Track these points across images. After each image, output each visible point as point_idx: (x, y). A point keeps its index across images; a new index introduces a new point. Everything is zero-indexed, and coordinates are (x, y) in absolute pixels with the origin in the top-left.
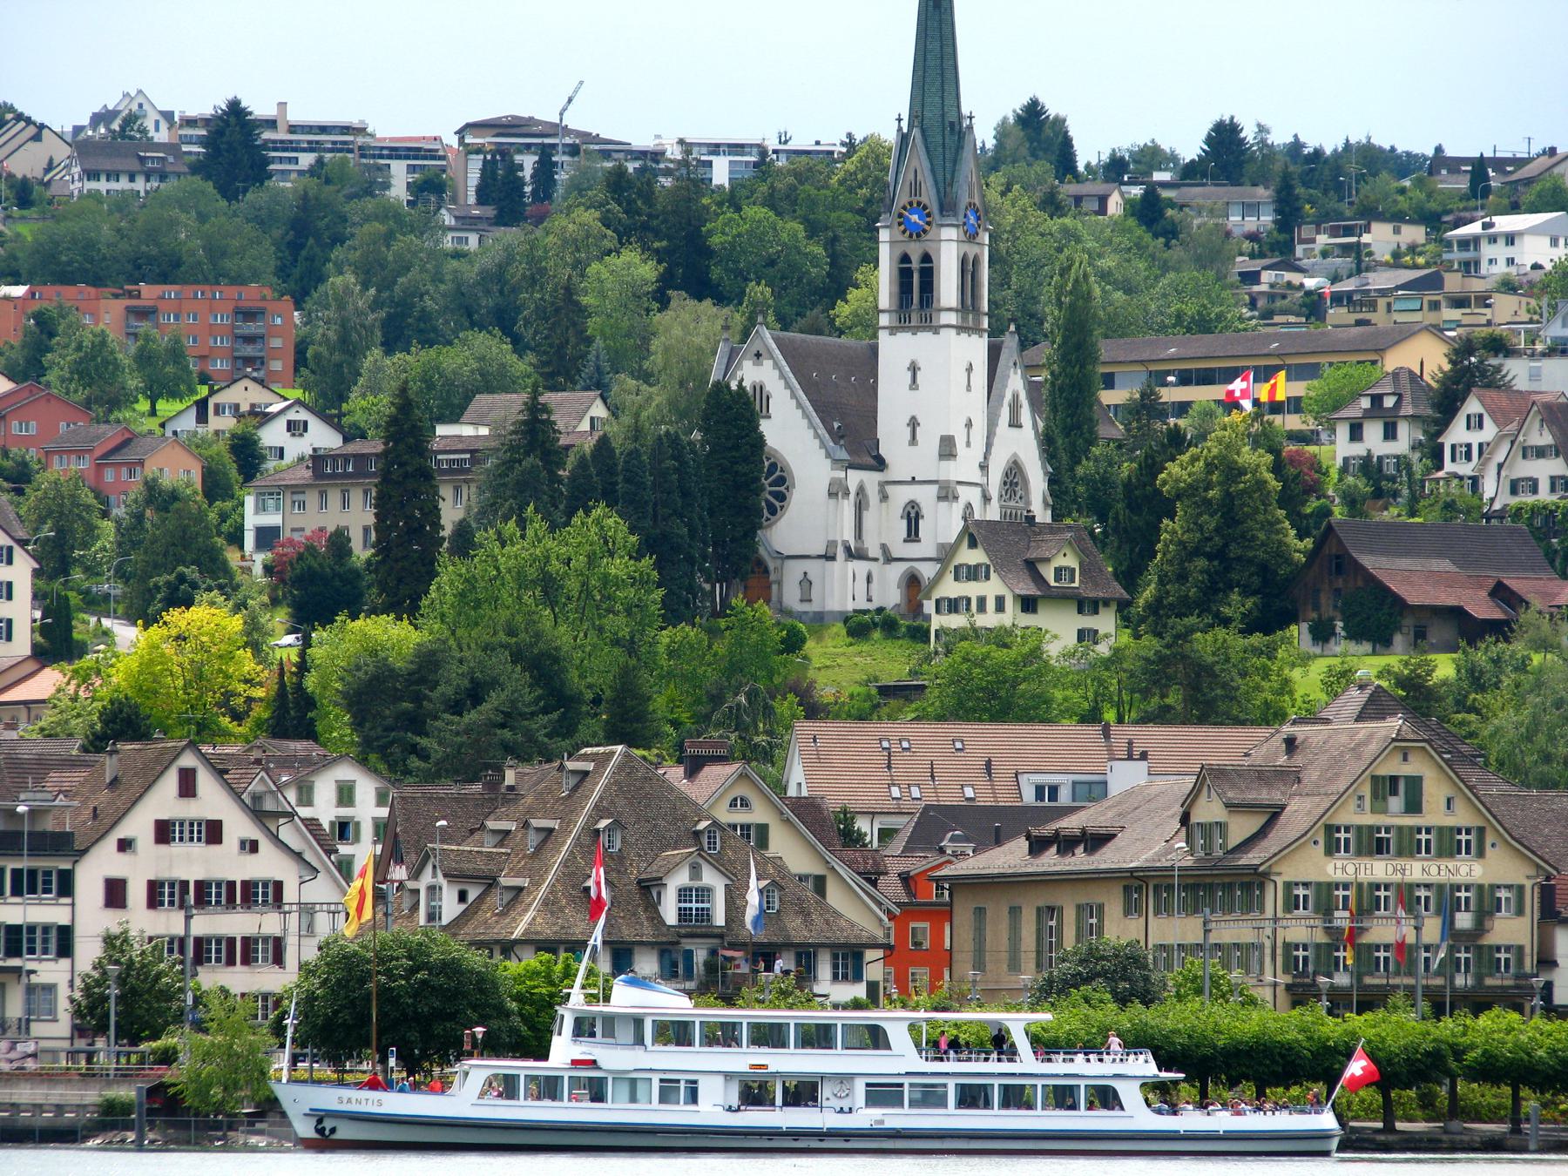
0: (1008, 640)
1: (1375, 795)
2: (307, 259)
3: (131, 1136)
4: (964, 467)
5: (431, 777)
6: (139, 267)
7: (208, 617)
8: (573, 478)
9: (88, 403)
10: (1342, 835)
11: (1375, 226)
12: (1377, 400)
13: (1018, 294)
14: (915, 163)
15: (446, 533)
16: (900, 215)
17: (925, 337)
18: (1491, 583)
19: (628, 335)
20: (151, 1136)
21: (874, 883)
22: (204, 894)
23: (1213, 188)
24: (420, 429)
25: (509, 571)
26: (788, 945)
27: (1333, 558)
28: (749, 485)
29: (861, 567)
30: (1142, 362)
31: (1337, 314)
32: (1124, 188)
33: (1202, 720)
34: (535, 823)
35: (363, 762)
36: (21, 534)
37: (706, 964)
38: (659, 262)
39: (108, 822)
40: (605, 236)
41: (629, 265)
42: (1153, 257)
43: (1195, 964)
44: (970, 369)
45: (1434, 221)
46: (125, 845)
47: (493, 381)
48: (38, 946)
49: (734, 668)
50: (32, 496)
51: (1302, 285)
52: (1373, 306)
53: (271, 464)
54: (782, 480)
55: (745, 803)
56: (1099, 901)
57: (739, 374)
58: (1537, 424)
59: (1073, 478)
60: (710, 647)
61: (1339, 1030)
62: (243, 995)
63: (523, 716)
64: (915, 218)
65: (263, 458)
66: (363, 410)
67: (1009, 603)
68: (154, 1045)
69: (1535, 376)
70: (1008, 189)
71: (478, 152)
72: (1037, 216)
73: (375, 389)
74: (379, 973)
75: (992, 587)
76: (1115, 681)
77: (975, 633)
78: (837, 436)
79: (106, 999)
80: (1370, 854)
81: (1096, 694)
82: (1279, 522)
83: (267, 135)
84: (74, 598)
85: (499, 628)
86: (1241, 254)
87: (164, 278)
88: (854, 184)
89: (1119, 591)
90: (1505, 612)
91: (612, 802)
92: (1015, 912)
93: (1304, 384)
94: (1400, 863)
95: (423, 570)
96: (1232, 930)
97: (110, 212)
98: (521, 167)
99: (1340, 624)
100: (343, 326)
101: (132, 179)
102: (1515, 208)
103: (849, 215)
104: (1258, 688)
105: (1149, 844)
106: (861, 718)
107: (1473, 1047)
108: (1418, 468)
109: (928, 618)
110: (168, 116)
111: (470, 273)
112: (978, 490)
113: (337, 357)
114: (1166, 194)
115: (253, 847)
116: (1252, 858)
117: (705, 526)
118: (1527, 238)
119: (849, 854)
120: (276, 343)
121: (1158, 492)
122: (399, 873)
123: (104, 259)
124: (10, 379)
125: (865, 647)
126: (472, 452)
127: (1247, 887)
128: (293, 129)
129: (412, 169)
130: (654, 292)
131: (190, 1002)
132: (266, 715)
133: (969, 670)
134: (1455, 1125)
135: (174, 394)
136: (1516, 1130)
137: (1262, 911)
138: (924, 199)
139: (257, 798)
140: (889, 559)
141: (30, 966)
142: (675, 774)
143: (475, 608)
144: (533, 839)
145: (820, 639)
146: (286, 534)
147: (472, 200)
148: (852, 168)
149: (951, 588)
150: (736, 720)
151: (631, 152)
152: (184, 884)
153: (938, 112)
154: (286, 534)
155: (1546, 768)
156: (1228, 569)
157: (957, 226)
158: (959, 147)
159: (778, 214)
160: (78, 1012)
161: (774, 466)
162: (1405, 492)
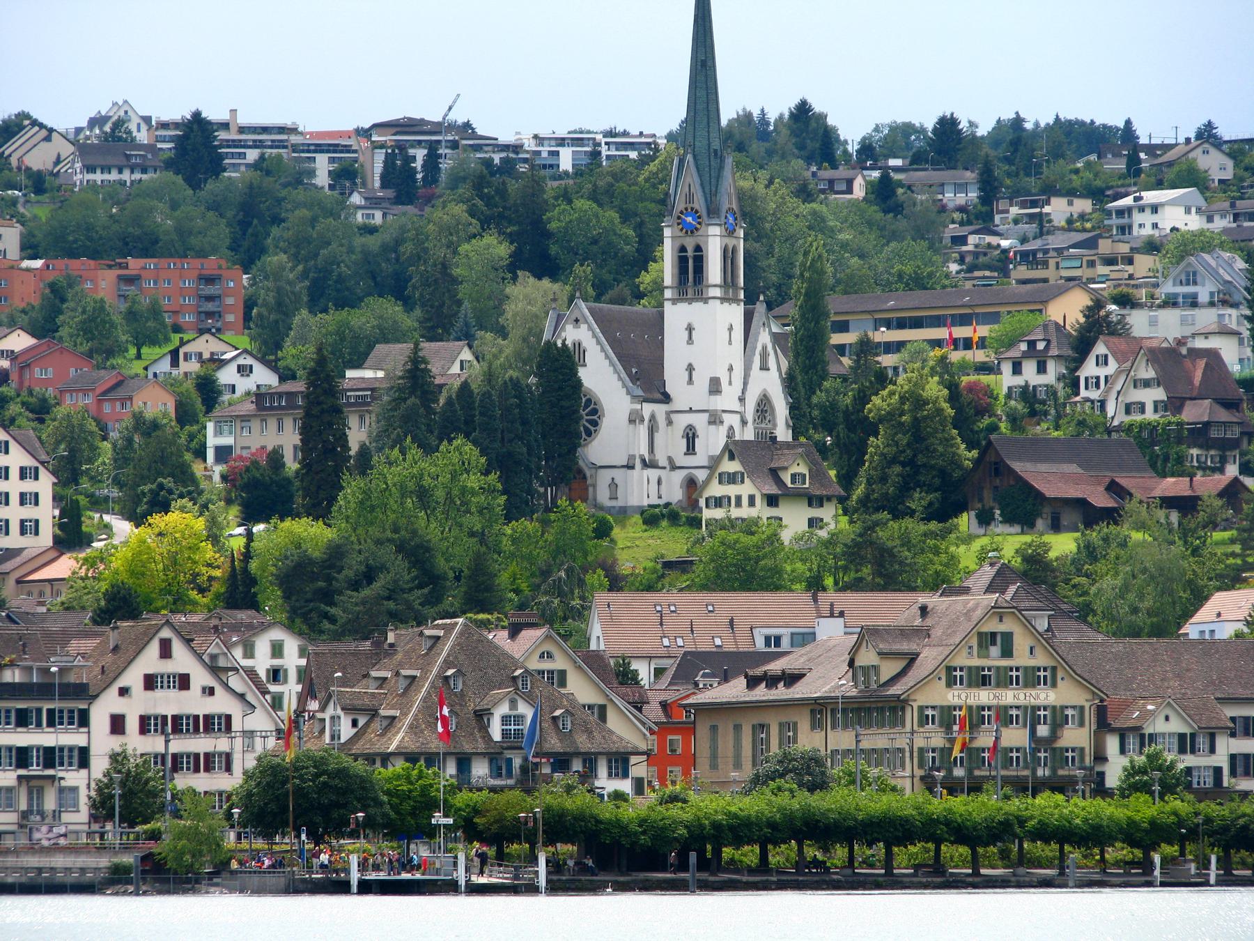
0: (754, 529)
1: (980, 645)
2: (252, 235)
3: (131, 888)
4: (728, 400)
5: (337, 637)
6: (127, 244)
7: (180, 520)
9: (90, 354)
10: (958, 673)
11: (1054, 200)
12: (1032, 344)
13: (779, 261)
14: (689, 180)
15: (352, 453)
16: (679, 218)
17: (698, 306)
18: (1108, 480)
19: (489, 298)
20: (144, 888)
21: (640, 710)
22: (179, 725)
25: (395, 485)
26: (577, 754)
27: (993, 466)
28: (571, 416)
29: (653, 474)
30: (869, 312)
31: (1022, 272)
32: (865, 172)
33: (884, 588)
34: (404, 672)
35: (290, 627)
36: (44, 457)
37: (521, 767)
38: (511, 243)
39: (112, 675)
41: (488, 246)
42: (882, 229)
43: (851, 764)
44: (731, 329)
45: (1098, 195)
46: (124, 692)
47: (388, 335)
48: (66, 760)
49: (559, 551)
50: (50, 426)
51: (999, 245)
52: (1045, 264)
53: (226, 397)
55: (550, 656)
56: (794, 720)
57: (563, 334)
58: (1144, 364)
59: (809, 405)
61: (941, 807)
62: (206, 793)
63: (403, 590)
64: (689, 219)
65: (220, 393)
67: (758, 500)
68: (145, 827)
69: (1153, 323)
70: (771, 182)
72: (792, 202)
73: (303, 339)
74: (294, 777)
75: (746, 489)
77: (731, 524)
78: (634, 379)
79: (113, 796)
80: (977, 686)
81: (819, 566)
82: (954, 438)
83: (223, 135)
84: (83, 500)
85: (387, 527)
86: (953, 222)
87: (146, 253)
90: (1117, 502)
91: (456, 657)
92: (738, 728)
93: (987, 327)
94: (998, 692)
96: (876, 739)
97: (104, 200)
99: (998, 512)
101: (120, 172)
102: (1159, 185)
103: (653, 205)
104: (931, 562)
105: (828, 679)
106: (650, 588)
107: (1032, 817)
108: (1061, 393)
109: (701, 511)
110: (147, 120)
111: (373, 242)
115: (210, 691)
116: (895, 690)
117: (539, 446)
118: (1168, 209)
119: (623, 689)
120: (230, 301)
121: (867, 418)
122: (313, 705)
123: (101, 238)
124: (33, 336)
125: (656, 533)
126: (372, 390)
127: (894, 710)
128: (242, 130)
129: (332, 160)
130: (508, 265)
131: (169, 798)
132: (223, 590)
134: (1021, 871)
135: (154, 342)
136: (1062, 874)
137: (904, 726)
138: (696, 206)
139: (214, 657)
140: (674, 467)
141: (61, 774)
142: (500, 637)
143: (370, 512)
144: (402, 684)
145: (624, 527)
146: (237, 452)
147: (377, 184)
148: (655, 170)
149: (716, 490)
150: (558, 590)
151: (498, 146)
152: (165, 718)
153: (705, 142)
154: (237, 452)
155: (1133, 617)
156: (917, 473)
159: (600, 205)
160: (94, 805)
161: (589, 401)
162: (1053, 412)
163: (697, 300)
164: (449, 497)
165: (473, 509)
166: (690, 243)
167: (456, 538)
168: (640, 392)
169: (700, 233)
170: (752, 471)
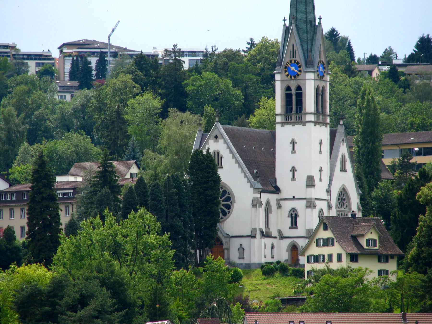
4: (318, 191)
8: (126, 199)
14: (293, 41)
17: (299, 127)
19: (148, 134)
23: (423, 66)
24: (50, 175)
25: (97, 242)
29: (268, 241)
32: (380, 67)
38: (162, 99)
40: (135, 87)
44: (321, 143)
47: (81, 156)
49: (208, 291)
54: (229, 199)
57: (207, 146)
60: (196, 280)
63: (106, 312)
64: (293, 68)
66: (19, 172)
67: (344, 257)
71: (70, 56)
73: (24, 161)
75: (336, 249)
76: (399, 295)
78: (256, 177)
81: (390, 301)
88: (255, 61)
89: (399, 251)
95: (51, 245)
98: (90, 63)
100: (9, 132)
103: (253, 76)
111: (69, 110)
112: (325, 203)
113: (6, 147)
114: (400, 70)
117: (191, 221)
125: (272, 280)
126: (74, 189)
129: (38, 65)
133: (329, 289)
138: (298, 59)
140: (282, 237)
143: (80, 260)
147: (67, 78)
149: (315, 250)
157: (314, 72)
158: (315, 33)
159: (219, 76)
161: (225, 192)
163: (298, 123)
164: (135, 250)
165: (152, 259)
166: (293, 85)
167: (140, 278)
168: (259, 186)
169: (300, 77)
170: (340, 237)
